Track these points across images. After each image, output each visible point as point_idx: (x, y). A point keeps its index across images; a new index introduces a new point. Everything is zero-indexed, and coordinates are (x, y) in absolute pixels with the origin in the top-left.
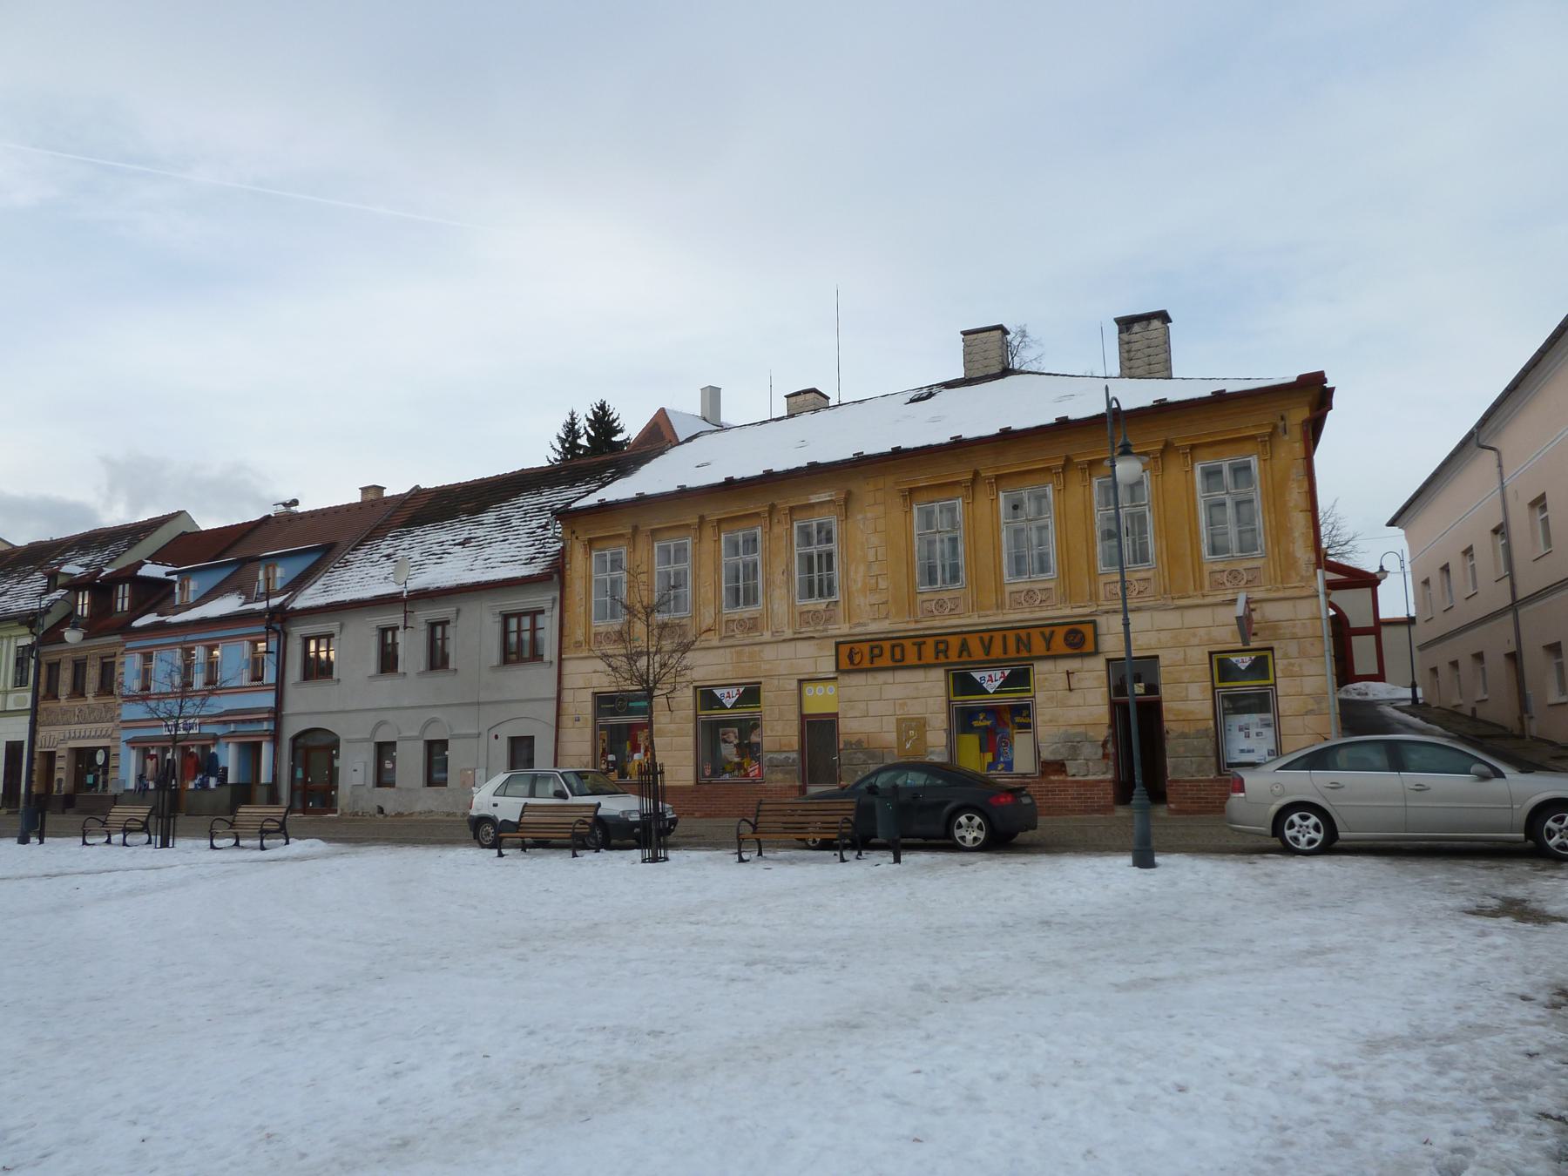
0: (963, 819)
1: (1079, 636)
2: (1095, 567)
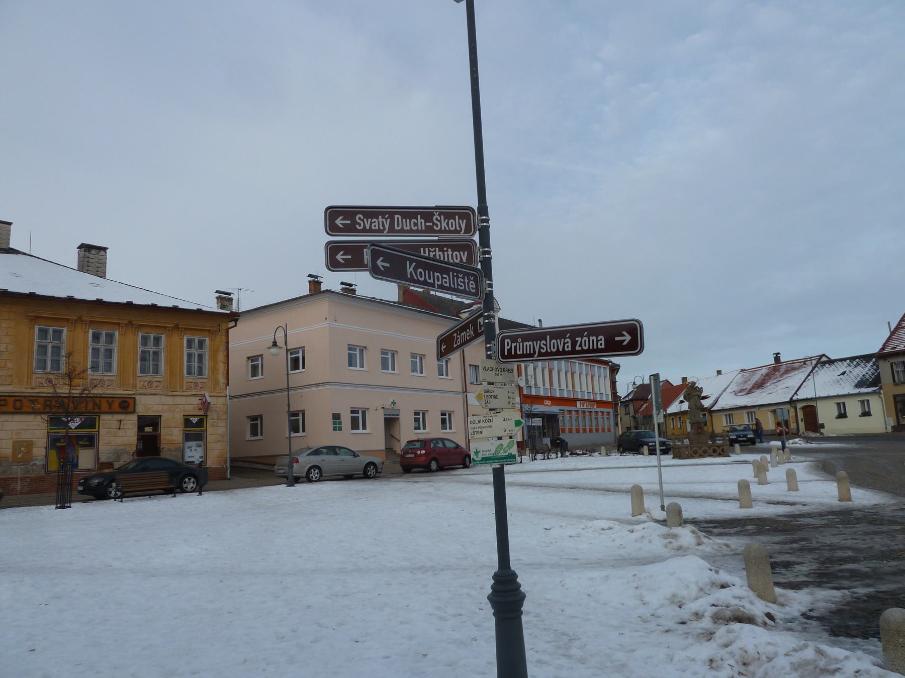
0: (187, 480)
1: (127, 404)
2: (136, 373)
